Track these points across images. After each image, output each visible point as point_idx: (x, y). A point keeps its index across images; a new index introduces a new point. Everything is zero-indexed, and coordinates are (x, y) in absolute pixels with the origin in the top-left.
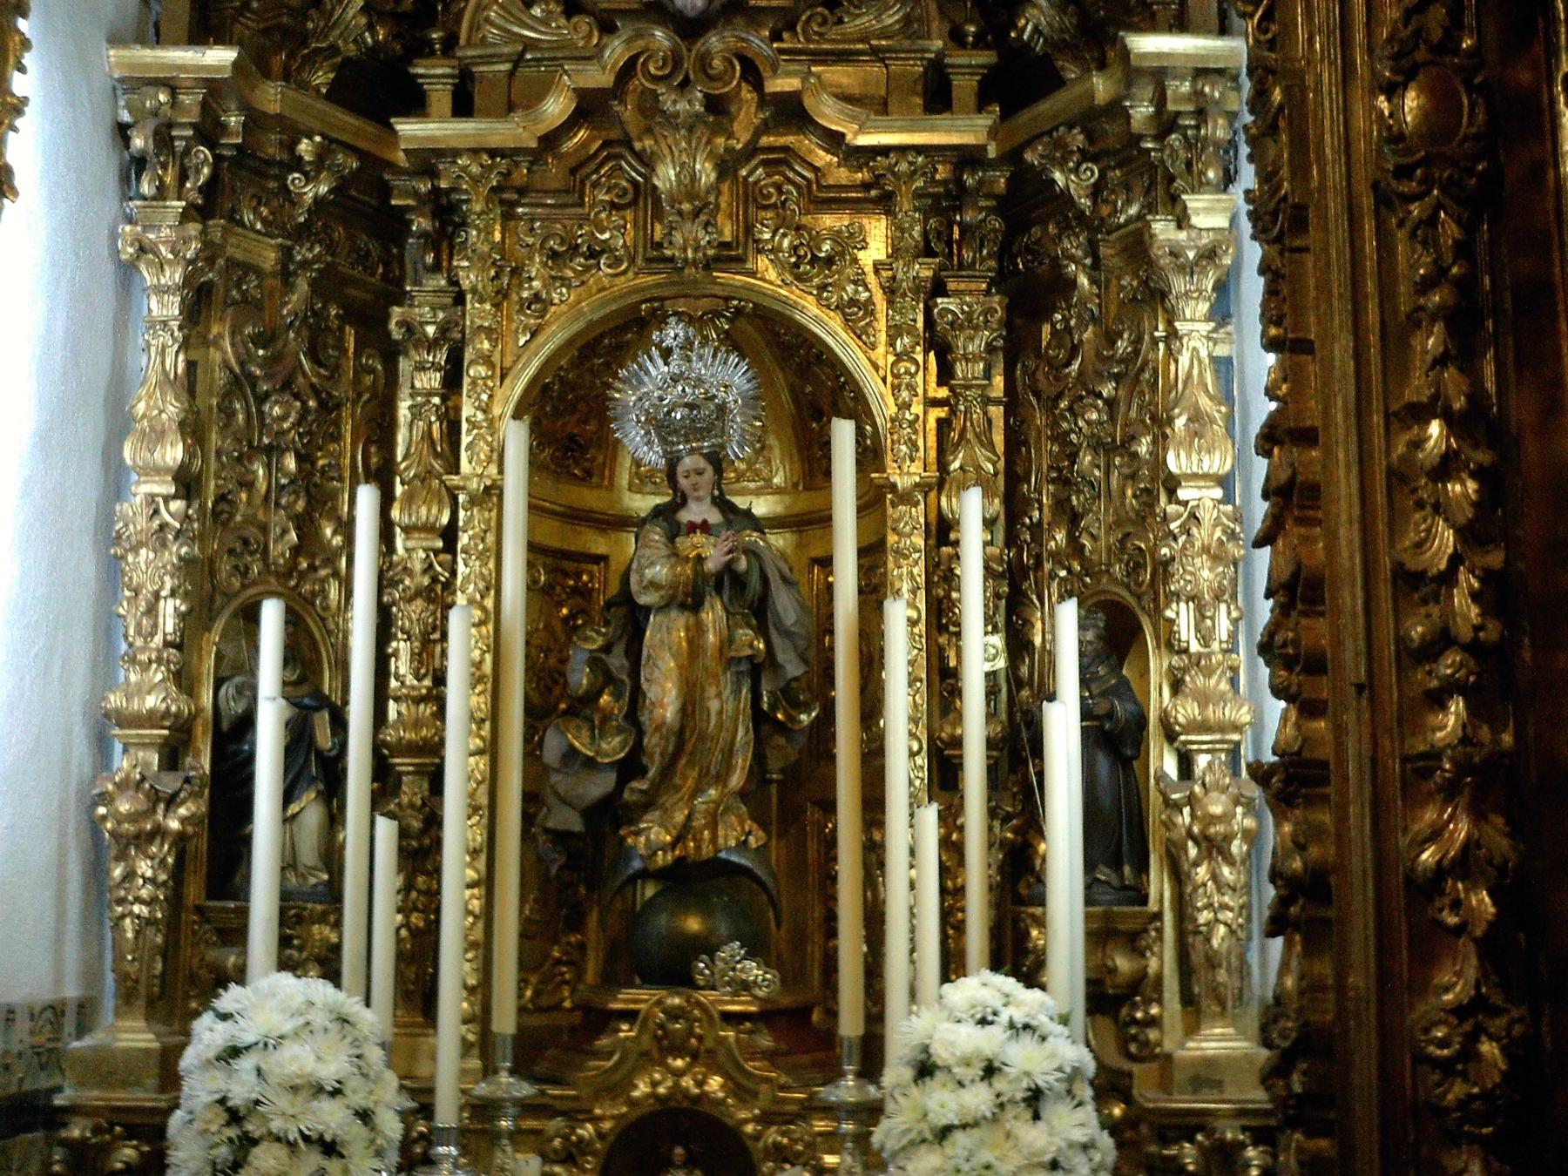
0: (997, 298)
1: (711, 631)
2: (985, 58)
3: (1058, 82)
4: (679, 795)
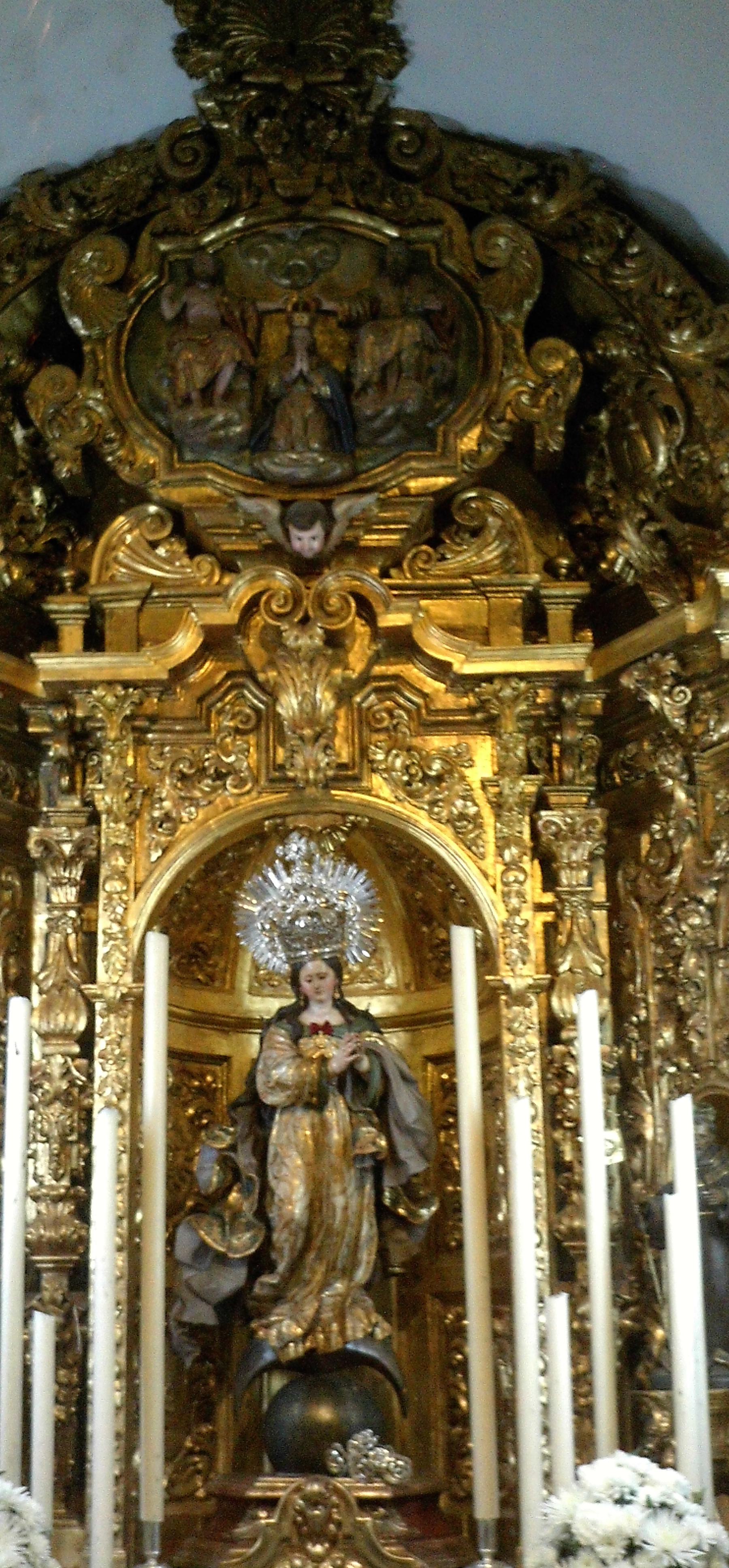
0: (598, 811)
1: (335, 1128)
2: (580, 589)
3: (649, 614)
4: (308, 1289)
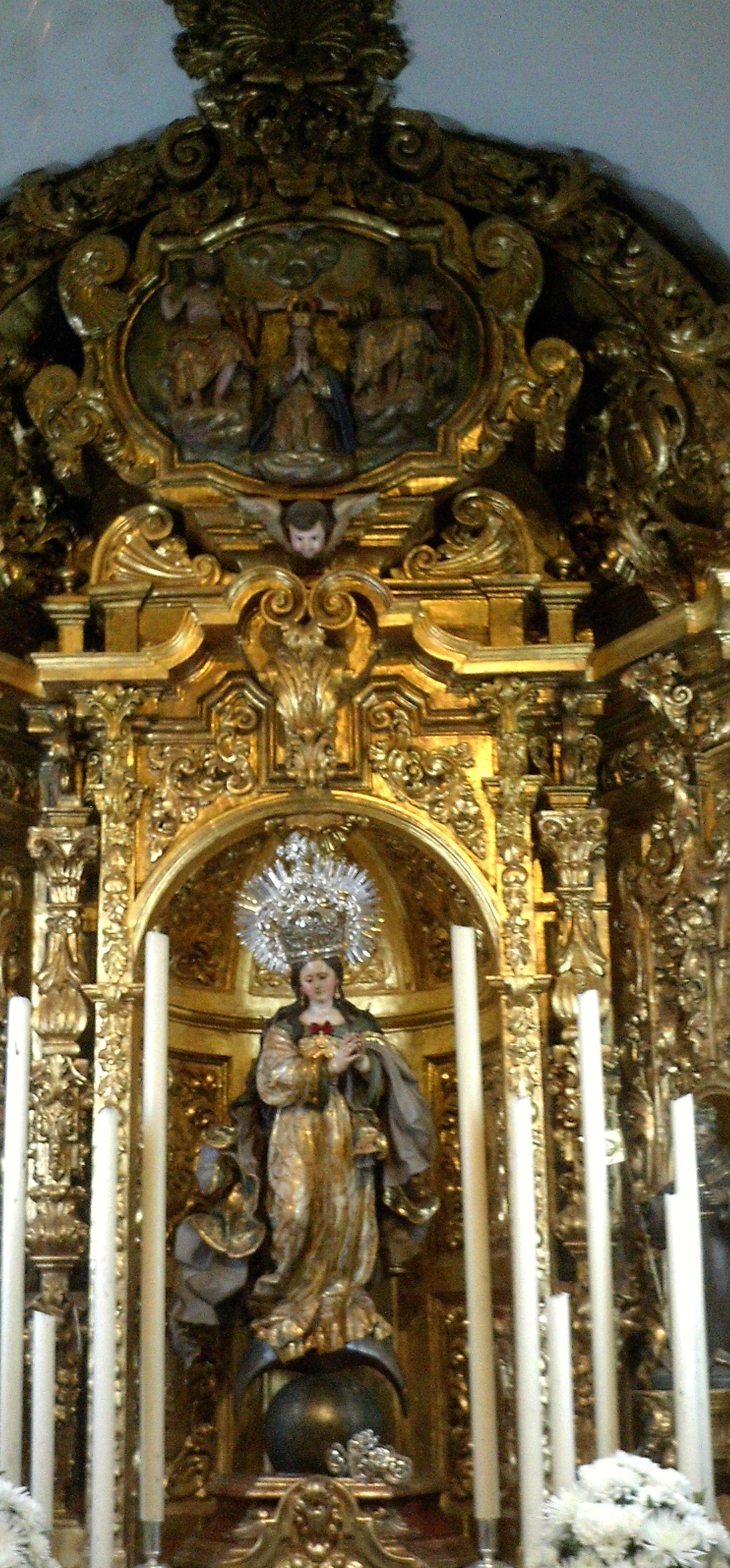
0: (599, 811)
1: (336, 1128)
2: (581, 589)
3: (650, 614)
4: (309, 1289)
